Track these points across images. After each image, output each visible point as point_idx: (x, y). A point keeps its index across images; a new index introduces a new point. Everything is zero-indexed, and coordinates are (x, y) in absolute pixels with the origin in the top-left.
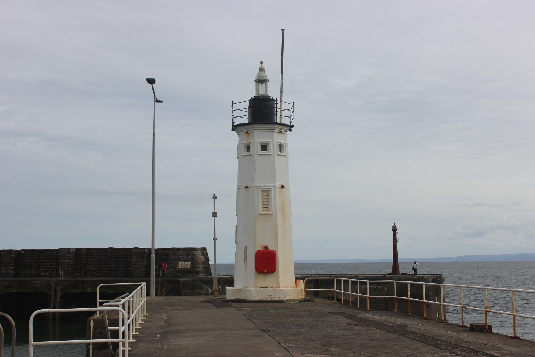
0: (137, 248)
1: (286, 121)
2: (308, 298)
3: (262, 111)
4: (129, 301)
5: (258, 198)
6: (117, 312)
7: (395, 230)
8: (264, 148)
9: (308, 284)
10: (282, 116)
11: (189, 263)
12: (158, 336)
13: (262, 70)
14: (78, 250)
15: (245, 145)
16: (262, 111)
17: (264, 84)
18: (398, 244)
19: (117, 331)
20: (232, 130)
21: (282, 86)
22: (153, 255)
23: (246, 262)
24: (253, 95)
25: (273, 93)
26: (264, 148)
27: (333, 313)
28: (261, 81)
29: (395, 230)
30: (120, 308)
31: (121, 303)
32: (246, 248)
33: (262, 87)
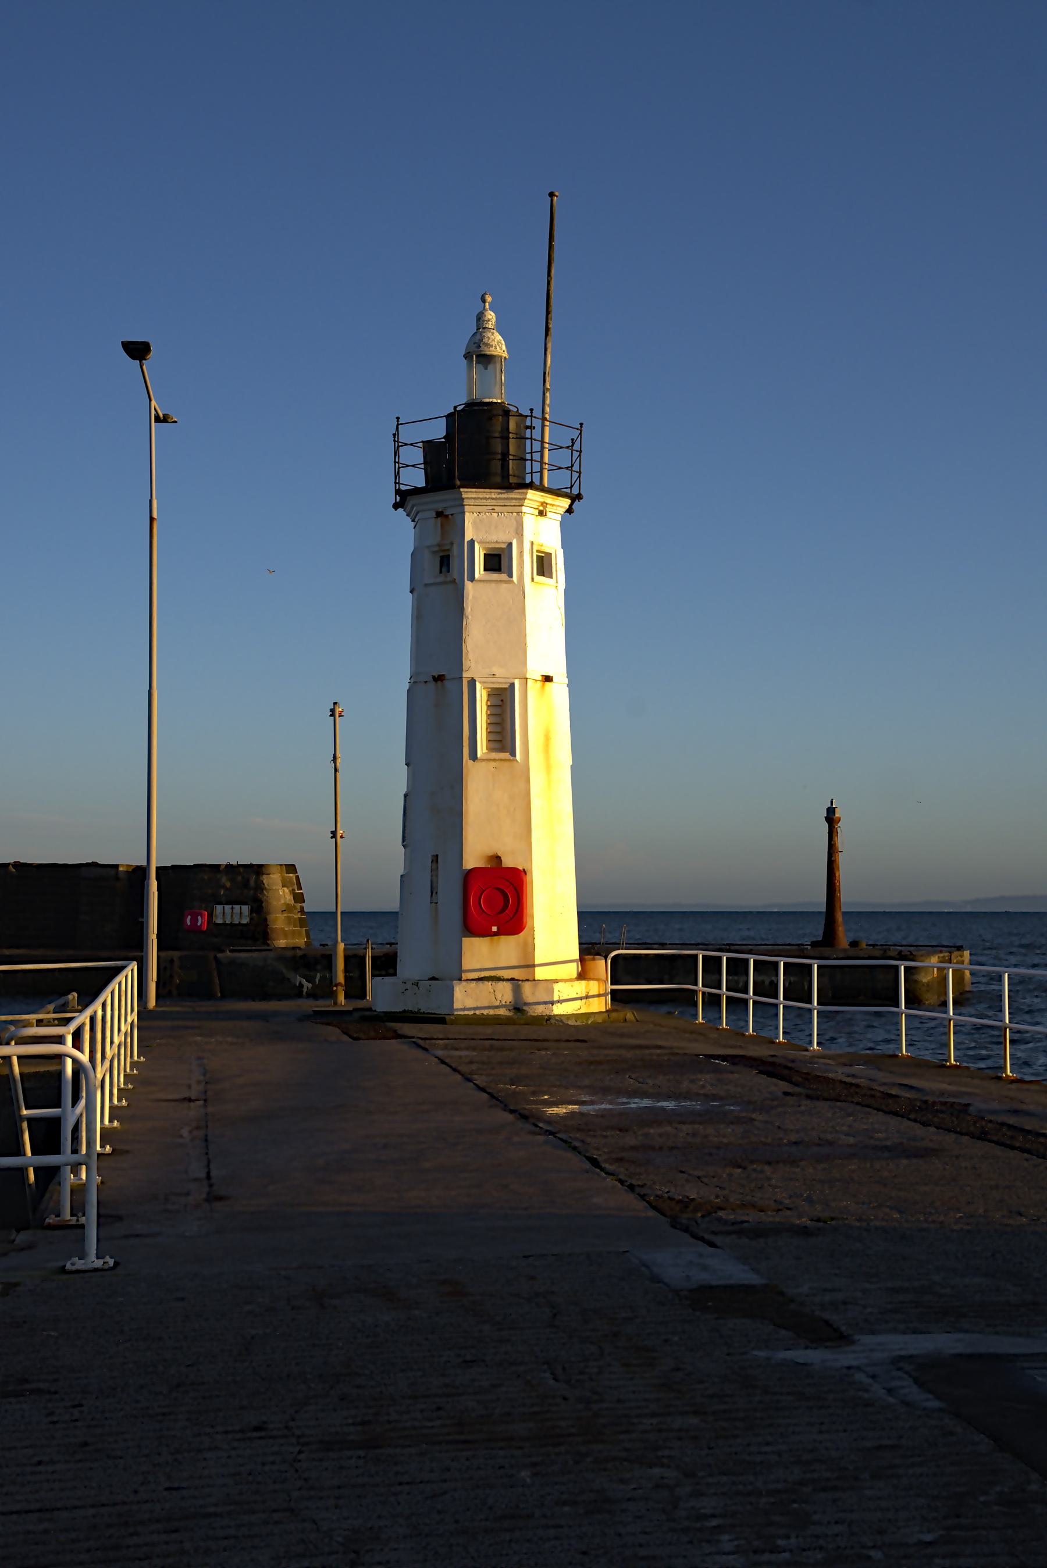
0: (94, 865)
4: (93, 1019)
6: (59, 1058)
9: (620, 970)
11: (246, 909)
12: (185, 1132)
19: (55, 1123)
20: (396, 506)
24: (460, 400)
30: (68, 1047)
31: (73, 1027)
32: (435, 859)
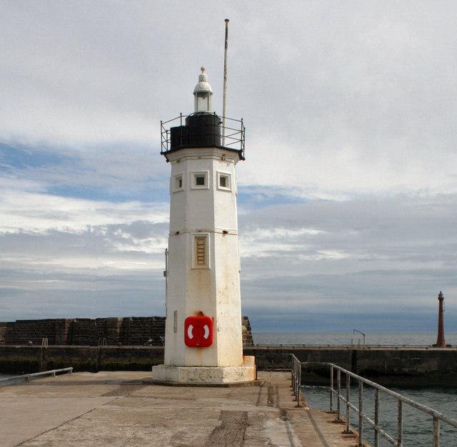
7: (441, 299)
8: (201, 181)
15: (177, 179)
17: (206, 98)
21: (224, 97)
23: (175, 332)
29: (441, 299)
33: (202, 102)
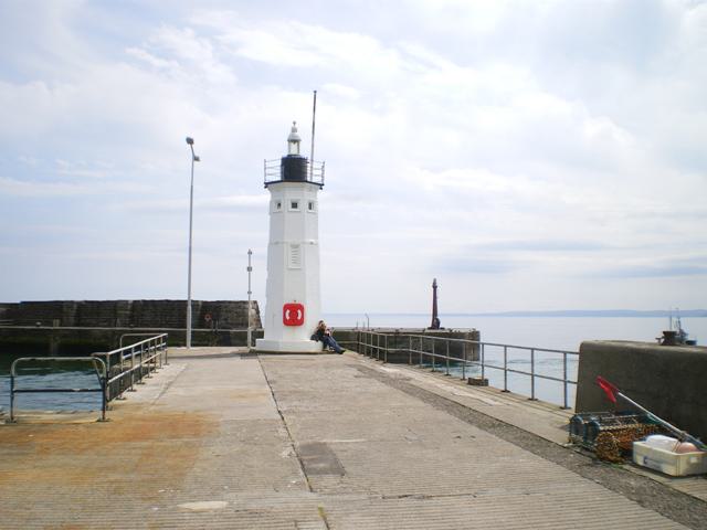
1: (316, 179)
2: (342, 349)
3: (294, 169)
5: (286, 250)
7: (435, 287)
8: (295, 205)
10: (313, 174)
13: (294, 130)
14: (135, 301)
16: (294, 169)
18: (438, 300)
22: (190, 307)
24: (285, 154)
25: (304, 152)
26: (295, 205)
27: (350, 366)
28: (294, 141)
29: (435, 287)
33: (294, 146)
